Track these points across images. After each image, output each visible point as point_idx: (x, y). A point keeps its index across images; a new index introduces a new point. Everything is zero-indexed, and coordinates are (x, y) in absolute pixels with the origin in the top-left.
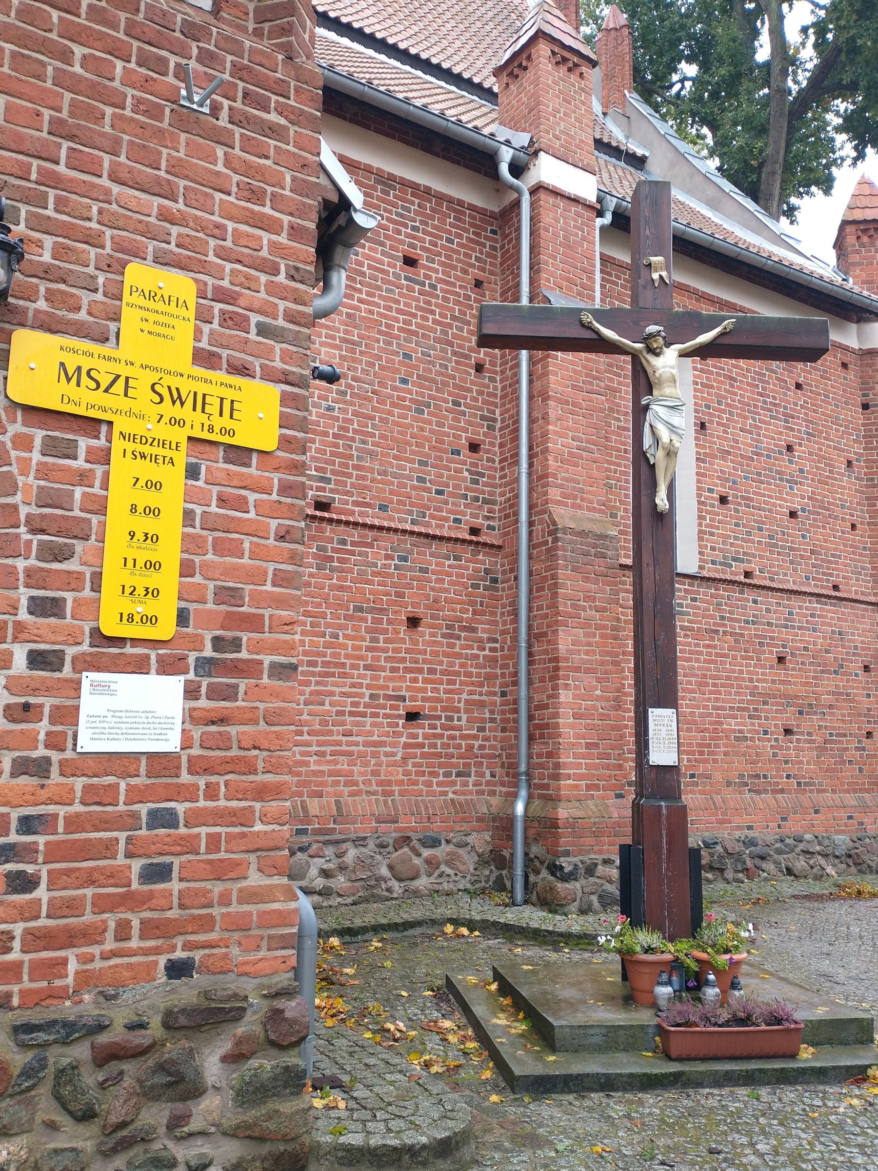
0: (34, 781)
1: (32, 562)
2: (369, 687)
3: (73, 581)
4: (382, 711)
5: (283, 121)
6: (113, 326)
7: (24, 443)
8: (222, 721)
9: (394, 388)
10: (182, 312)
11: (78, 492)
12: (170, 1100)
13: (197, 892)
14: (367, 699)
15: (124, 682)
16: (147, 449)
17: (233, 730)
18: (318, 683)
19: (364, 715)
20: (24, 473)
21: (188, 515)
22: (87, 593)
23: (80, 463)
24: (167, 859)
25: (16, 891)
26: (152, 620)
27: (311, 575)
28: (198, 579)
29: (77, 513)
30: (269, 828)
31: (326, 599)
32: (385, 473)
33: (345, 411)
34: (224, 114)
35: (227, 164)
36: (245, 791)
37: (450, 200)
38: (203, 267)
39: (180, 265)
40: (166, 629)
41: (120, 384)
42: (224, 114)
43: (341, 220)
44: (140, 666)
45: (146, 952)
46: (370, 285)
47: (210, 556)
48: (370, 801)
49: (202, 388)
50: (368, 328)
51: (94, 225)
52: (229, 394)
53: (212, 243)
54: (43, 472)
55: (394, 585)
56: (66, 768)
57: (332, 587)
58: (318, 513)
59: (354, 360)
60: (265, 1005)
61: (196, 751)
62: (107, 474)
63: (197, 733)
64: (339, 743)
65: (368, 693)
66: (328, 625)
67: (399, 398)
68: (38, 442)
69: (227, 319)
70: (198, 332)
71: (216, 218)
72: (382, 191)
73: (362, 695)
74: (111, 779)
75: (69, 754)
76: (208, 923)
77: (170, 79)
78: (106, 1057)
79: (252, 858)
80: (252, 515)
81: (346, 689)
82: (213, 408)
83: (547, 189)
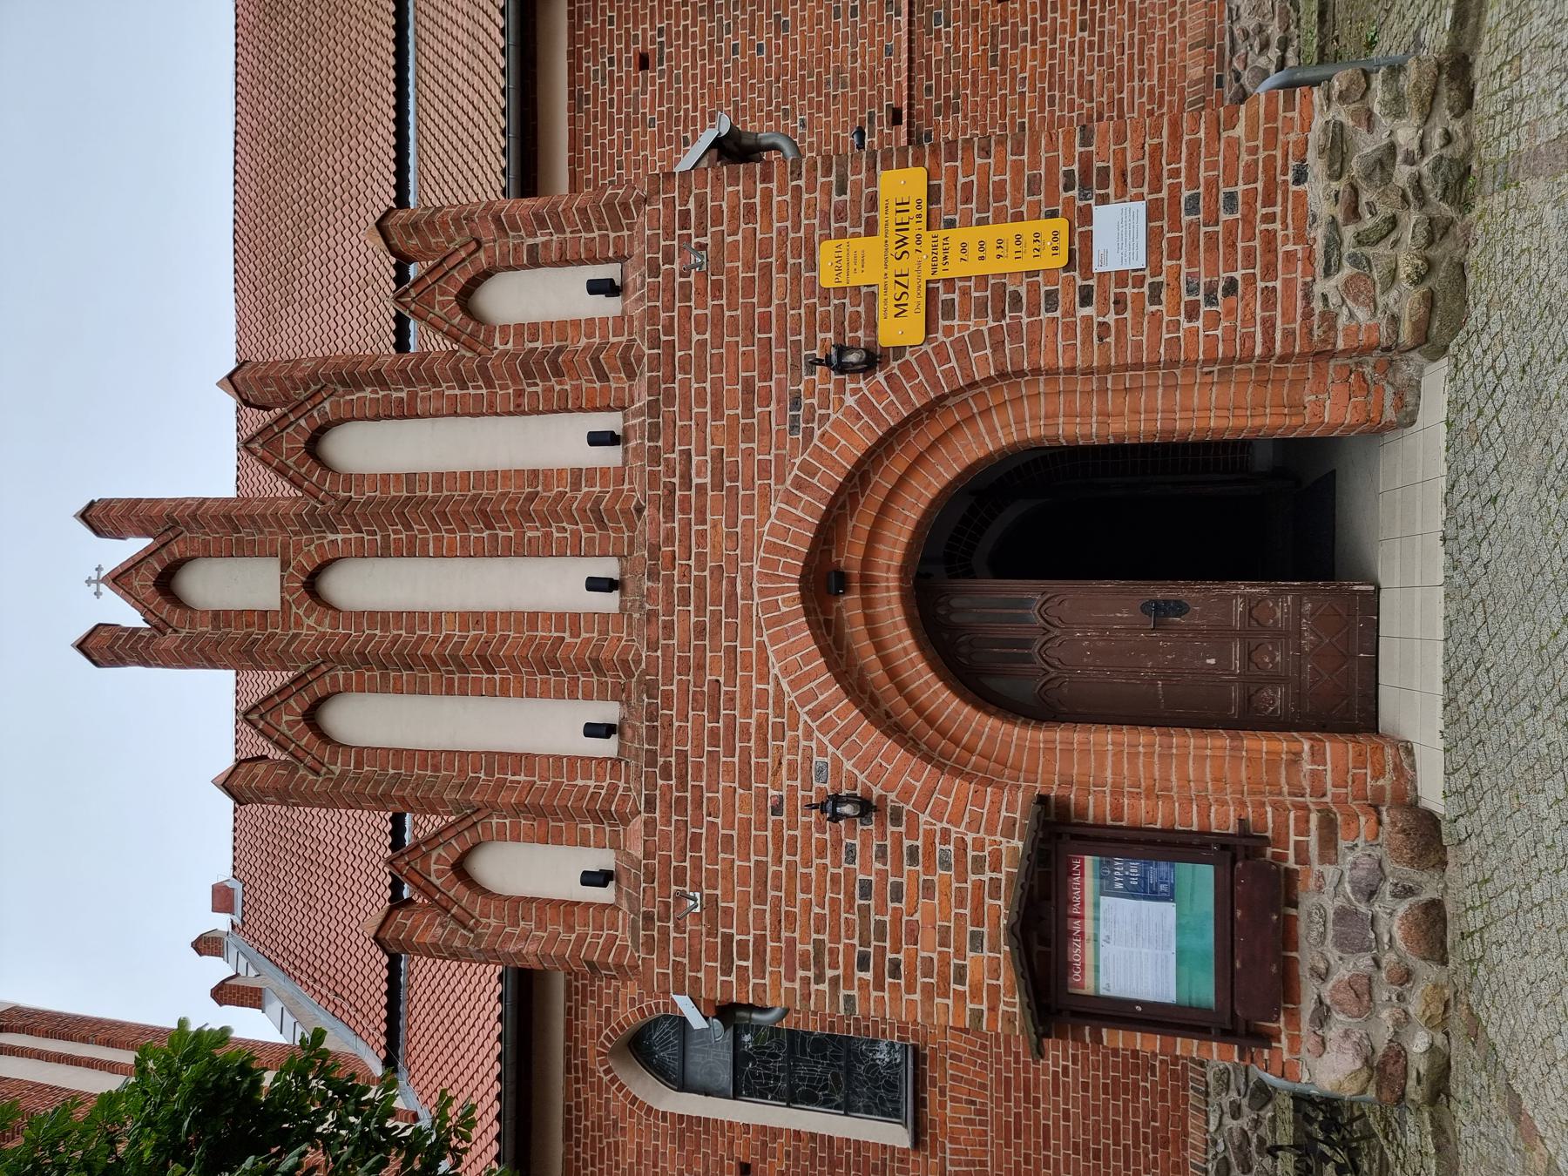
0: (1164, 290)
1: (1023, 314)
2: (1073, 35)
3: (1034, 288)
4: (1098, 14)
5: (692, 199)
6: (864, 290)
7: (948, 331)
8: (1124, 174)
9: (769, 60)
10: (844, 248)
11: (975, 294)
12: (1394, 165)
13: (1246, 172)
14: (1086, 34)
15: (1098, 246)
16: (940, 256)
17: (1130, 165)
18: (1071, 92)
19: (1102, 34)
20: (968, 327)
21: (980, 222)
22: (1040, 279)
23: (956, 296)
24: (1221, 196)
25: (1236, 290)
26: (1056, 235)
27: (965, 117)
28: (1024, 209)
29: (989, 293)
30: (1203, 126)
31: (986, 97)
32: (854, 55)
33: (802, 108)
34: (702, 240)
35: (735, 233)
36: (1175, 149)
37: (572, 28)
38: (809, 239)
39: (812, 254)
40: (1061, 224)
41: (902, 280)
42: (702, 240)
43: (729, 145)
44: (1087, 238)
45: (1285, 200)
46: (678, 102)
47: (1007, 203)
48: (1192, 11)
49: (892, 227)
50: (719, 97)
51: (802, 311)
52: (893, 207)
53: (791, 235)
54: (965, 316)
55: (966, 25)
56: (1157, 272)
57: (975, 94)
58: (905, 120)
59: (752, 107)
60: (1335, 106)
61: (1145, 189)
62: (961, 279)
63: (1132, 191)
64: (1131, 57)
65: (1079, 34)
66: (1013, 91)
67: (777, 52)
68: (947, 323)
69: (840, 216)
70: (854, 235)
71: (774, 235)
72: (587, 103)
73: (1082, 40)
74: (1165, 244)
75: (1147, 272)
76: (1270, 160)
77: (692, 279)
78: (1353, 213)
79: (1224, 135)
80: (974, 178)
81: (1076, 59)
82: (904, 217)
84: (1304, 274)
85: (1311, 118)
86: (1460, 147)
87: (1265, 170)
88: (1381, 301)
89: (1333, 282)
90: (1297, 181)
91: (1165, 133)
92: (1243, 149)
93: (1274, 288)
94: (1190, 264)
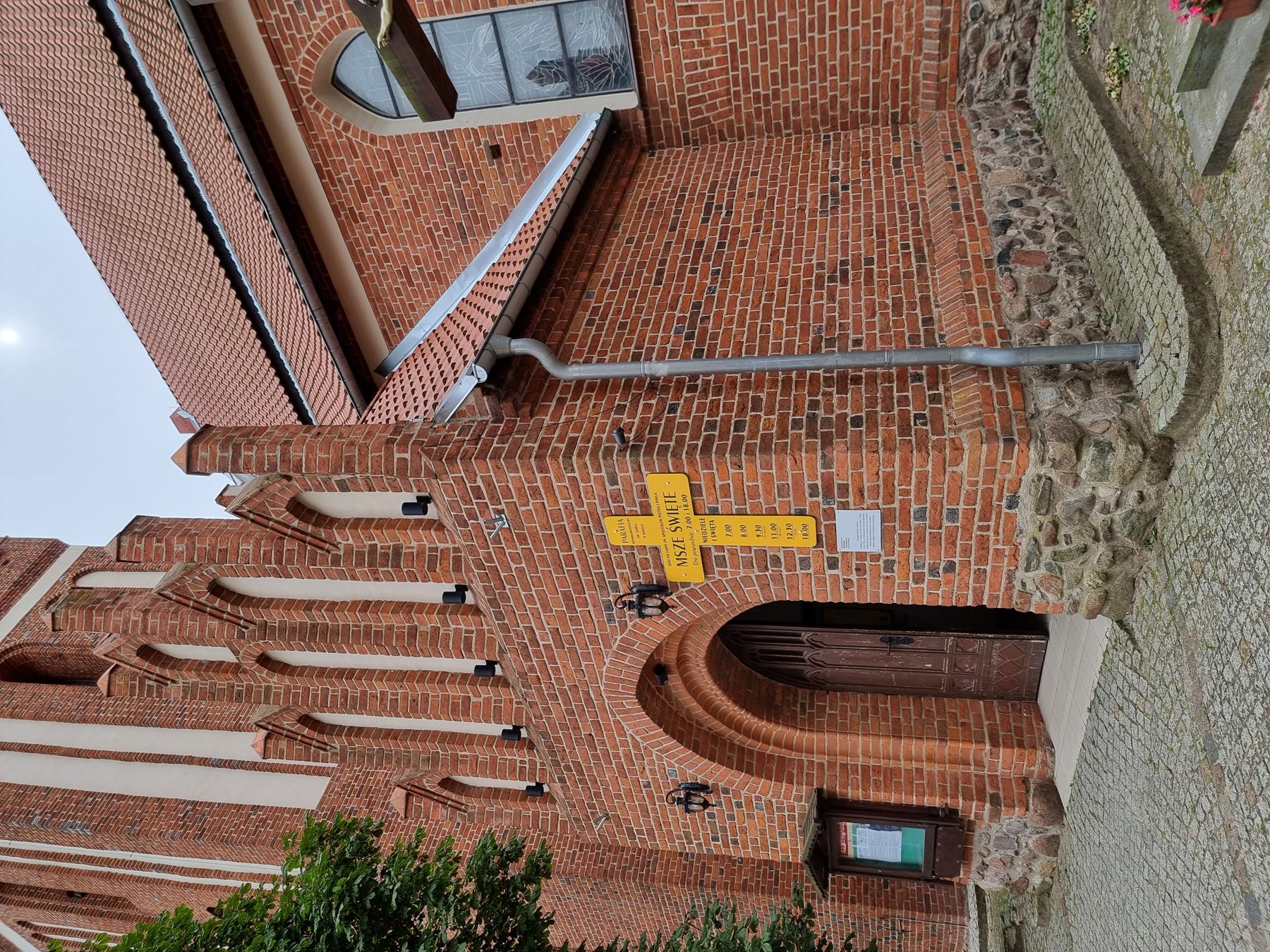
16: (709, 532)
17: (866, 485)
24: (945, 511)
26: (805, 527)
49: (664, 512)
52: (662, 499)
61: (880, 501)
63: (868, 501)
84: (1009, 564)
85: (1026, 467)
86: (1150, 505)
87: (983, 497)
88: (1066, 592)
89: (1031, 574)
90: (1010, 507)
91: (897, 464)
92: (965, 482)
93: (985, 571)
94: (917, 551)
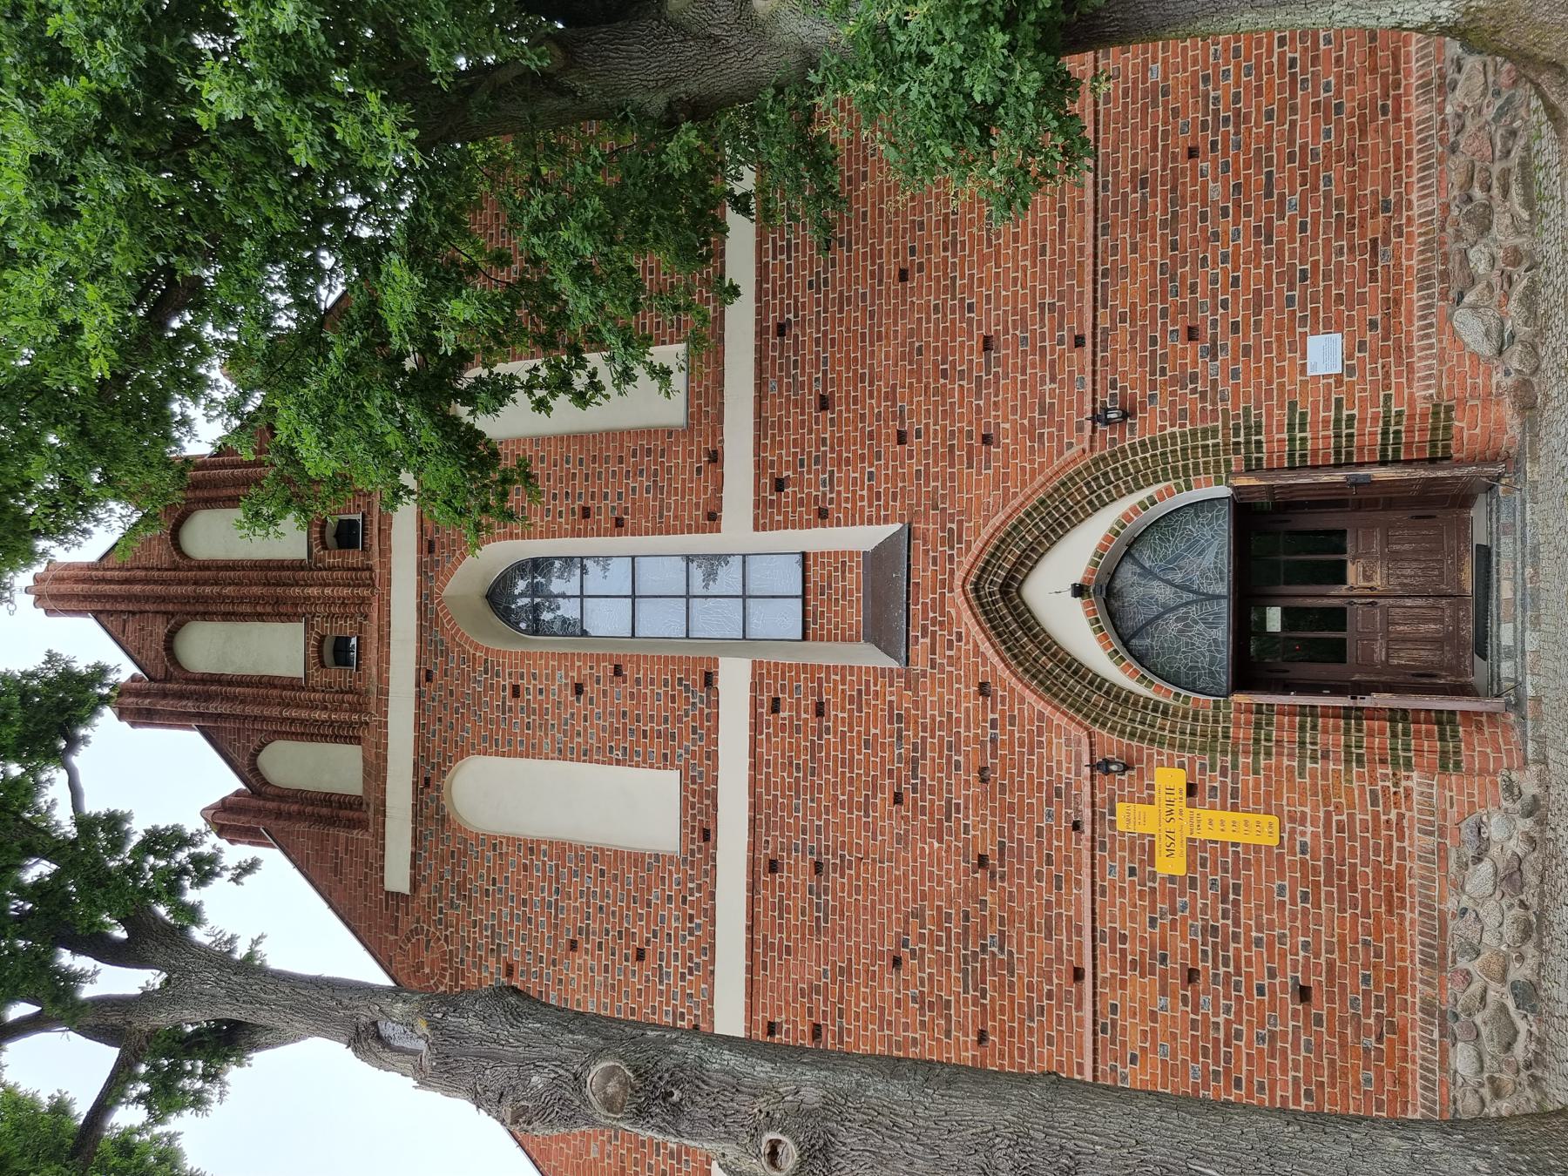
26: (1270, 825)
52: (1163, 791)
82: (1172, 797)
83: (1136, 540)
